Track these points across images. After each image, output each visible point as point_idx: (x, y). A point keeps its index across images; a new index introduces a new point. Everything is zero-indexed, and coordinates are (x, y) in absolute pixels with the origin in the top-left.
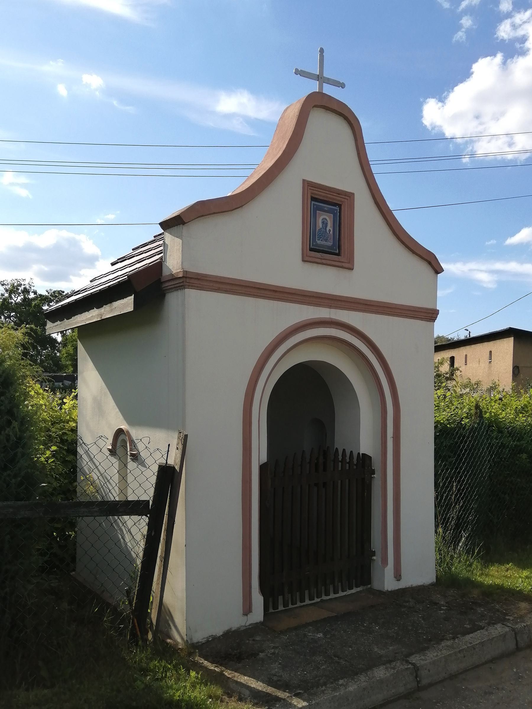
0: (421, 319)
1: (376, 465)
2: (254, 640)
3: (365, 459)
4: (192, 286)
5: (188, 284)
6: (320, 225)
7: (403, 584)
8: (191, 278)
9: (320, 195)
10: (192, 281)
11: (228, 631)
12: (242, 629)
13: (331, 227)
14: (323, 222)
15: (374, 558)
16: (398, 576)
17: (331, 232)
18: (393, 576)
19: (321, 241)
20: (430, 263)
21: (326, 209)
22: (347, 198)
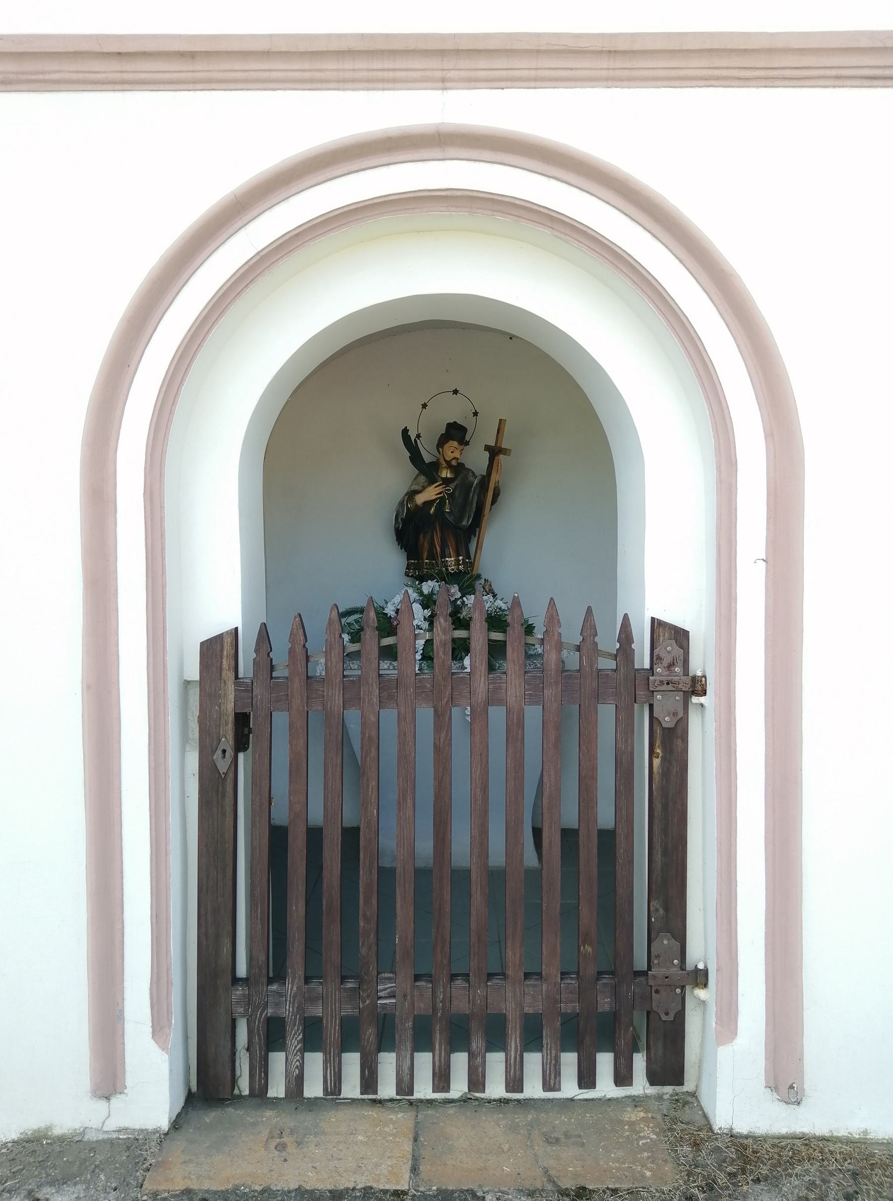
1: (700, 660)
12: (91, 1136)
15: (701, 993)
16: (786, 1085)
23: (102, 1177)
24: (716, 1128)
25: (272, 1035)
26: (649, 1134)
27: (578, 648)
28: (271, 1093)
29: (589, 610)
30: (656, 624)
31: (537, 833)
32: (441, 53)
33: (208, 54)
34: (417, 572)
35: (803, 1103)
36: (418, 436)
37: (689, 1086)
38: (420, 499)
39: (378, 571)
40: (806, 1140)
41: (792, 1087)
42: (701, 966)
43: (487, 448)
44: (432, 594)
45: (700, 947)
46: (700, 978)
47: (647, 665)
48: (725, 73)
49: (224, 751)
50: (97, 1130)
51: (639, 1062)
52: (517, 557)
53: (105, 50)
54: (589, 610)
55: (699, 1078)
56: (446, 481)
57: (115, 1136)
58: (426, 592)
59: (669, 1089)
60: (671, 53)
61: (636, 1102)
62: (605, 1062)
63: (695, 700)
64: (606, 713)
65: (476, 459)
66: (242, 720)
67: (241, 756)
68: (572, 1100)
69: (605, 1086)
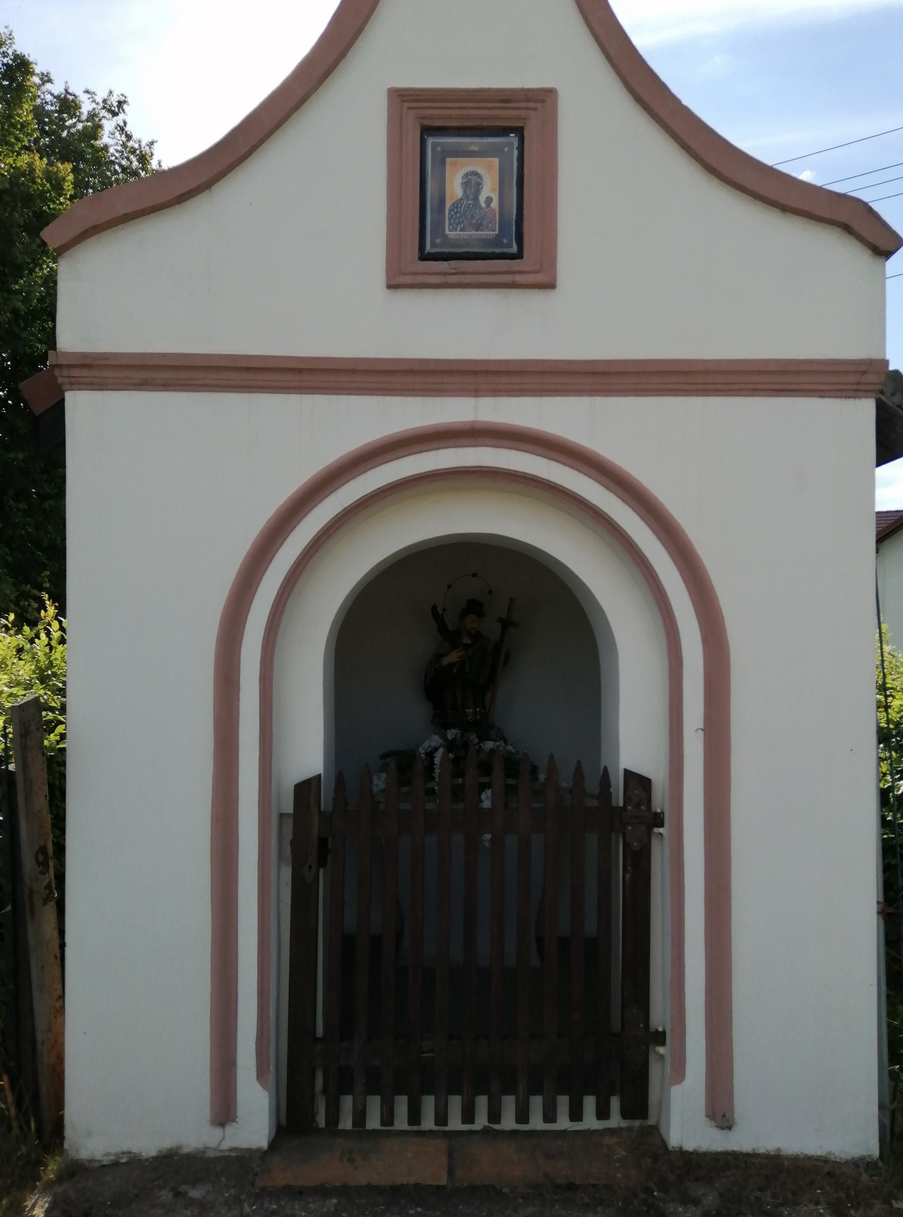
0: (821, 393)
1: (660, 800)
2: (178, 1194)
3: (638, 783)
4: (79, 384)
5: (66, 380)
6: (455, 189)
7: (740, 1141)
8: (69, 366)
9: (450, 118)
10: (76, 373)
11: (170, 1150)
12: (211, 1154)
13: (493, 190)
14: (466, 184)
15: (661, 1050)
16: (721, 1114)
17: (495, 205)
18: (703, 1113)
19: (462, 230)
20: (847, 229)
21: (473, 148)
22: (531, 105)
23: (224, 1179)
24: (670, 1148)
25: (341, 1084)
26: (621, 1152)
27: (571, 791)
28: (341, 1126)
29: (579, 762)
30: (628, 774)
31: (540, 940)
32: (475, 373)
33: (312, 371)
34: (441, 722)
35: (733, 1128)
36: (444, 610)
37: (652, 1121)
38: (446, 661)
39: (407, 718)
40: (735, 1155)
41: (724, 1116)
42: (660, 1029)
43: (500, 620)
44: (454, 740)
45: (659, 1017)
46: (660, 1038)
47: (621, 804)
48: (675, 387)
49: (310, 867)
50: (215, 1149)
51: (615, 1103)
52: (524, 710)
53: (239, 365)
54: (579, 762)
55: (659, 1115)
56: (466, 647)
57: (227, 1154)
58: (450, 737)
59: (637, 1123)
60: (637, 373)
61: (612, 1132)
62: (589, 1103)
63: (656, 830)
64: (592, 840)
65: (491, 628)
66: (323, 842)
67: (321, 871)
68: (565, 1131)
69: (590, 1122)
